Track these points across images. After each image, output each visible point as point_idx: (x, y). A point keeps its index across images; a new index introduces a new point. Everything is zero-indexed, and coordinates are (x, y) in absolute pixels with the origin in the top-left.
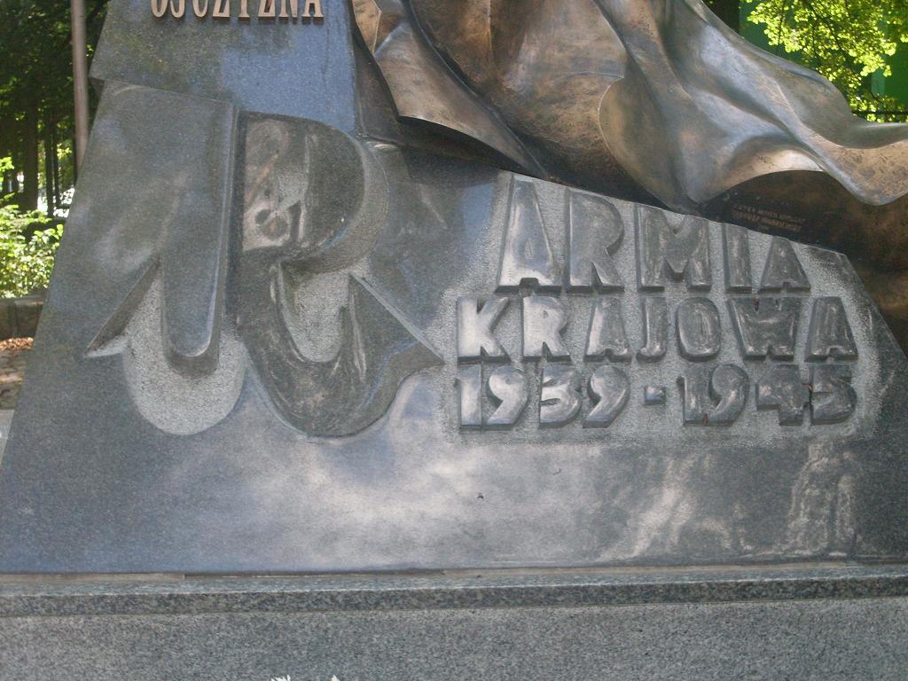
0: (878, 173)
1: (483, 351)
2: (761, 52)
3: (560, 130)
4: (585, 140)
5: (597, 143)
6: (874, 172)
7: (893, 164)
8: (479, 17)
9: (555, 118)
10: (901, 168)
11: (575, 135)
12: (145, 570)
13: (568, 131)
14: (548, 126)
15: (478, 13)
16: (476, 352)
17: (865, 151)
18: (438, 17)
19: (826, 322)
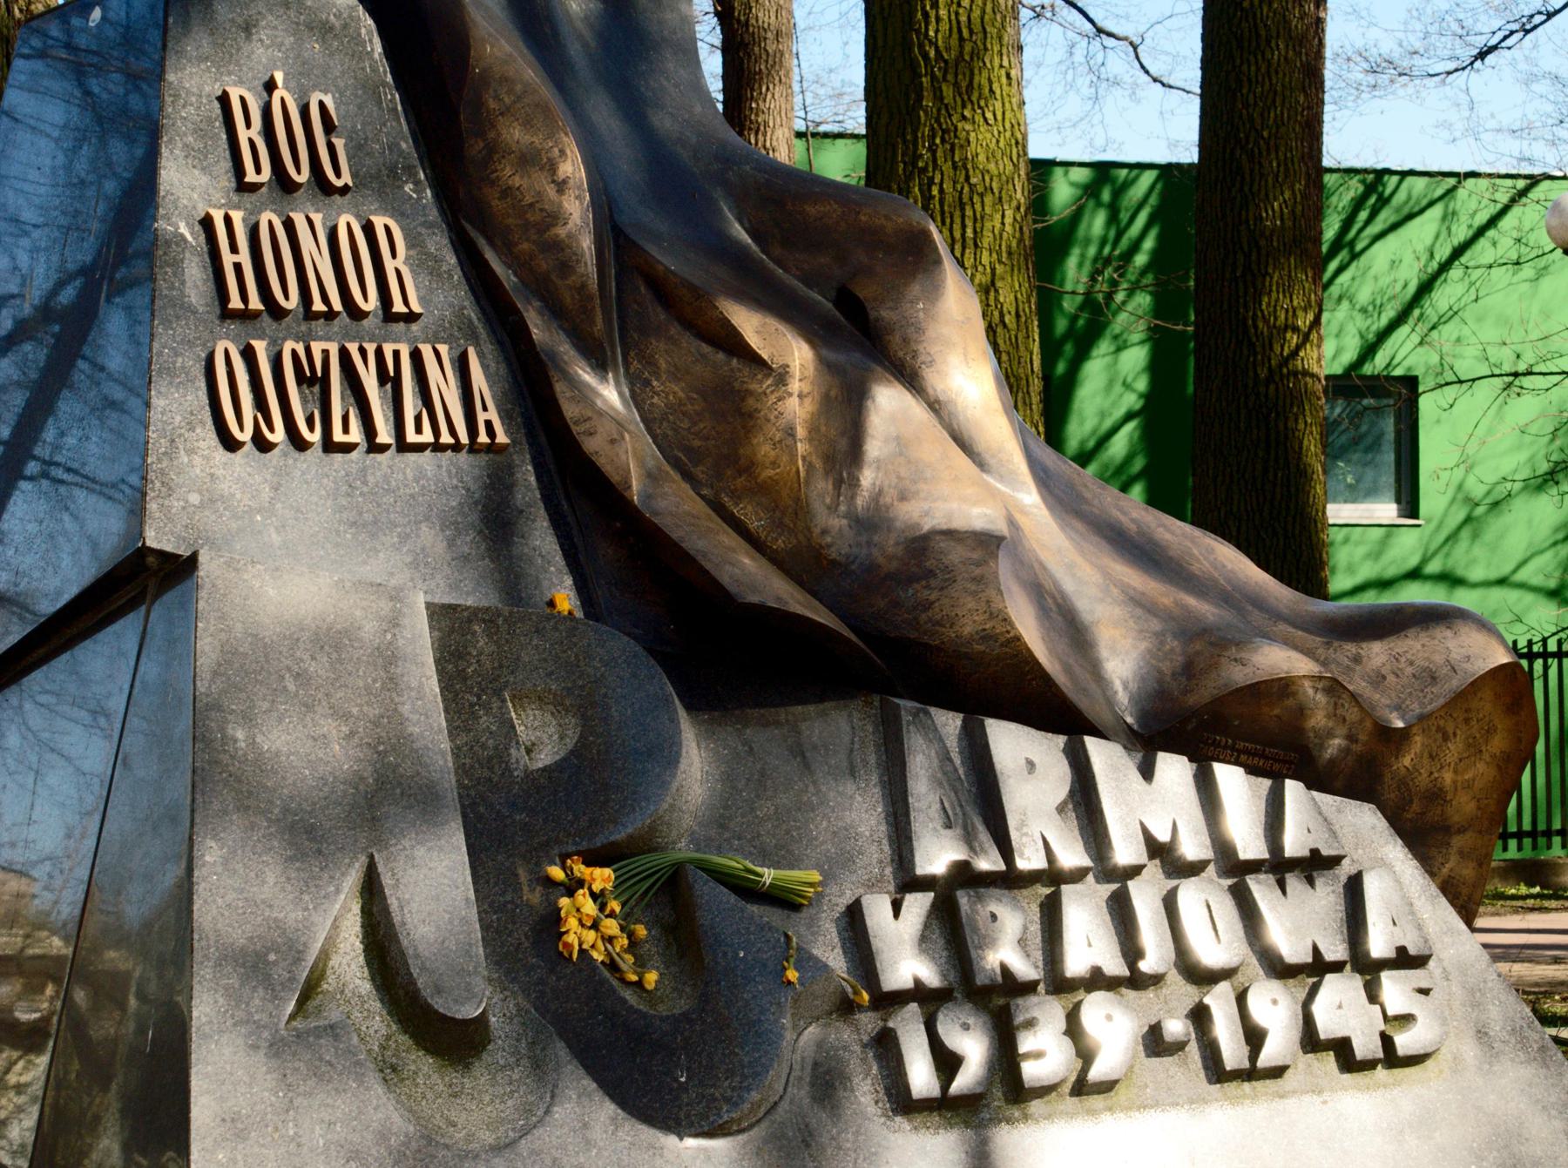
0: (1391, 678)
1: (917, 982)
2: (387, 420)
3: (939, 623)
4: (986, 637)
5: (1009, 641)
6: (1384, 677)
7: (1411, 663)
8: (780, 442)
9: (928, 606)
10: (1425, 669)
11: (967, 630)
12: (1482, 218)
13: (952, 625)
14: (915, 619)
15: (778, 436)
16: (910, 984)
17: (1364, 645)
18: (697, 443)
19: (1225, 307)
